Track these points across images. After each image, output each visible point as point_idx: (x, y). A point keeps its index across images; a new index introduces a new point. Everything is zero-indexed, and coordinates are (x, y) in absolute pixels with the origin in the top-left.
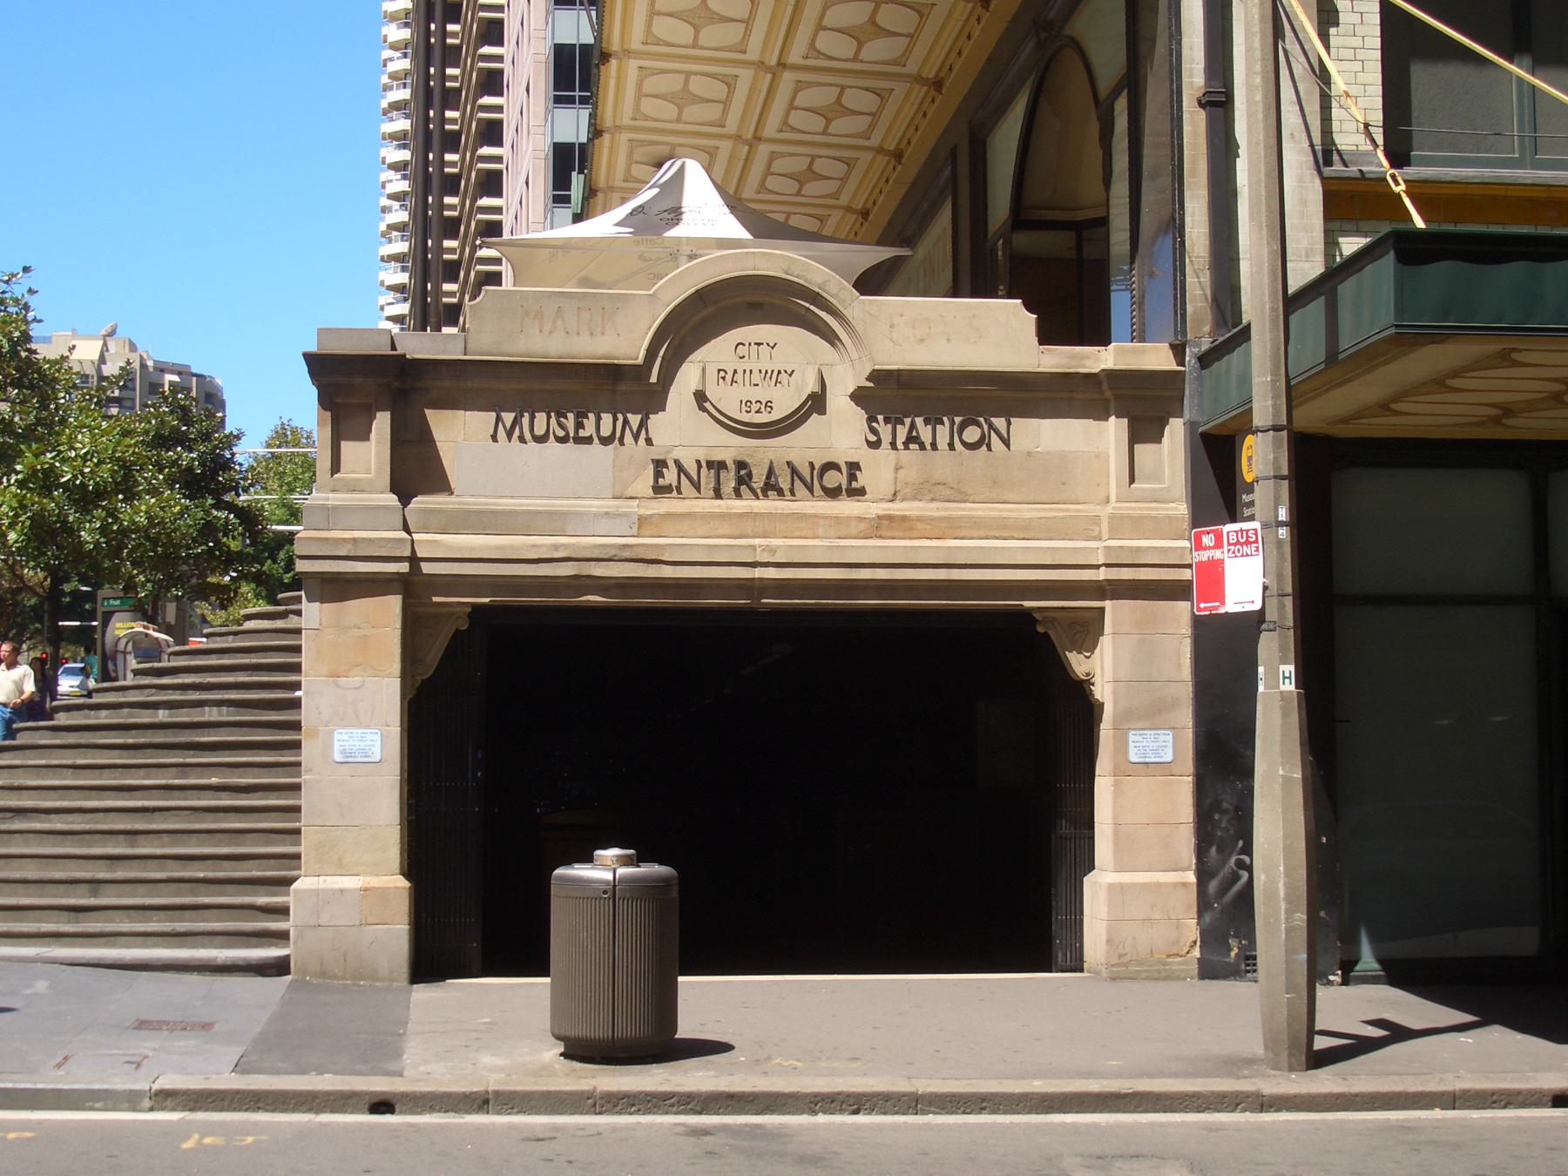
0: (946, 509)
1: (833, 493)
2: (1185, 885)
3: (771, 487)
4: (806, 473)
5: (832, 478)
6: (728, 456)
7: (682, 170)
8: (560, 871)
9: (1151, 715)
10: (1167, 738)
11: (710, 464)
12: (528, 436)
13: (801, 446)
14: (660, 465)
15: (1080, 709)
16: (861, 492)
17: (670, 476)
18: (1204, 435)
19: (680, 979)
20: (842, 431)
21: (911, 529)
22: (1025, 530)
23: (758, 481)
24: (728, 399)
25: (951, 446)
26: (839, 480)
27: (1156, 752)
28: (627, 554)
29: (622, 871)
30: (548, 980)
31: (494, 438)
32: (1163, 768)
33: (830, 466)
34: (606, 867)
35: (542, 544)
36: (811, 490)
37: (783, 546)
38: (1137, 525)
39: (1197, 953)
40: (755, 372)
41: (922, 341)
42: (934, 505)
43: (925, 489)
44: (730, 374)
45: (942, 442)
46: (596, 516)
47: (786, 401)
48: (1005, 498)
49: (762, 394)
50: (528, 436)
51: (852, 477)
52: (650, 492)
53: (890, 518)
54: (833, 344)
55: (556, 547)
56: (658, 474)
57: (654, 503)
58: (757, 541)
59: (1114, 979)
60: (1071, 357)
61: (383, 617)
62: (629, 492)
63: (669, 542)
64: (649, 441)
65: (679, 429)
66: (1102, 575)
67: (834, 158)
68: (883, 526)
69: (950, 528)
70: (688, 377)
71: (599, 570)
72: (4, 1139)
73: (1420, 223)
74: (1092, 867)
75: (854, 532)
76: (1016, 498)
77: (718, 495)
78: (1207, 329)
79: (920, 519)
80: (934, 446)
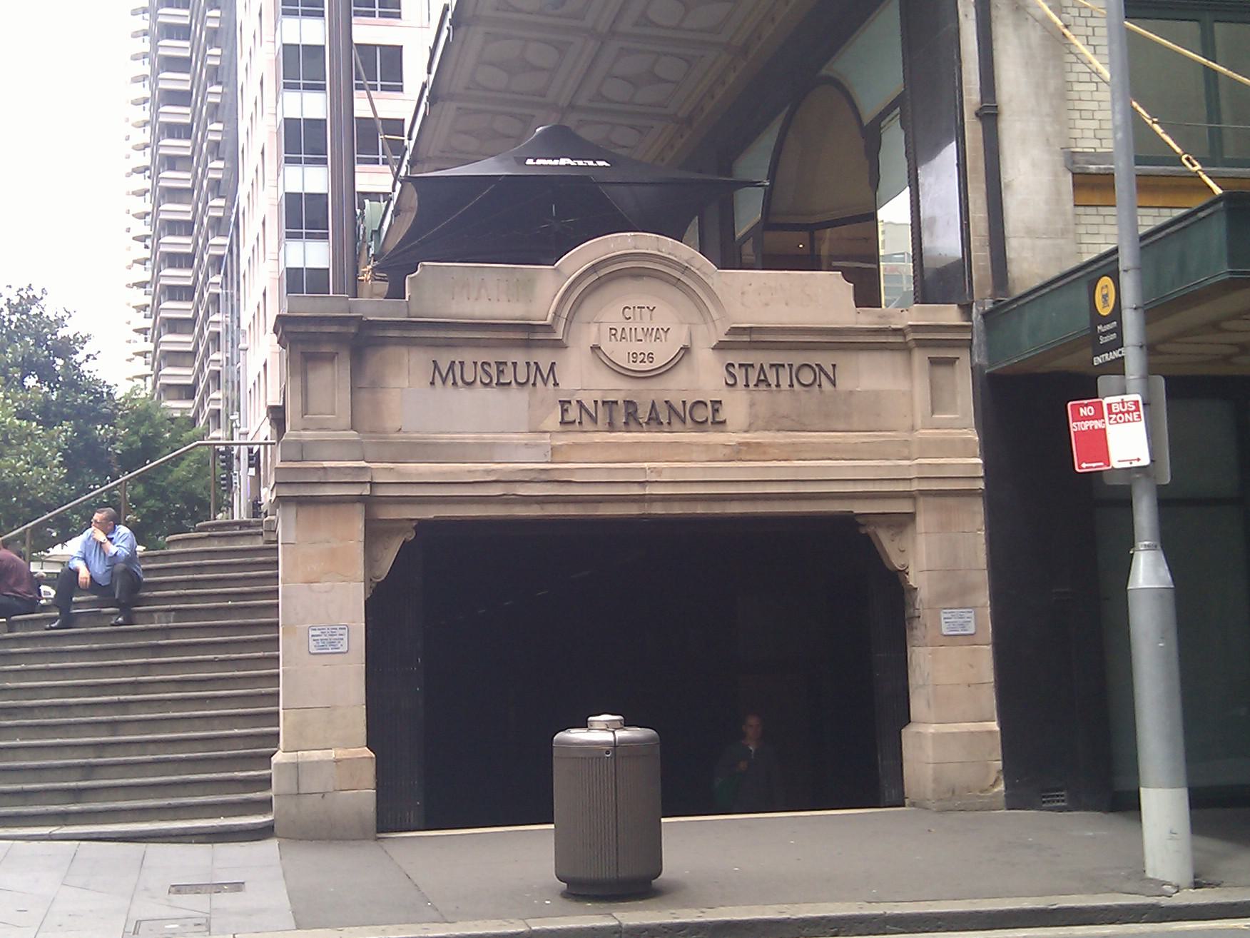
0: (790, 437)
1: (700, 425)
2: (991, 732)
3: (654, 421)
4: (680, 409)
5: (701, 414)
6: (619, 397)
8: (560, 736)
9: (956, 595)
10: (969, 615)
12: (460, 382)
13: (677, 388)
15: (895, 589)
17: (573, 413)
18: (991, 376)
19: (663, 820)
20: (705, 376)
21: (765, 453)
22: (853, 453)
23: (643, 413)
24: (619, 352)
25: (791, 385)
26: (705, 415)
27: (963, 626)
28: (544, 477)
29: (620, 734)
30: (552, 826)
31: (432, 383)
32: (969, 639)
34: (601, 731)
35: (475, 469)
36: (684, 421)
37: (666, 468)
38: (930, 447)
39: (1001, 787)
40: (639, 330)
41: (767, 305)
42: (780, 434)
43: (775, 422)
44: (620, 331)
45: (785, 383)
46: (517, 446)
47: (664, 352)
48: (835, 427)
49: (646, 347)
50: (460, 382)
51: (716, 411)
52: (558, 427)
53: (748, 444)
55: (488, 472)
56: (564, 411)
57: (563, 436)
58: (646, 465)
59: (943, 811)
61: (348, 534)
62: (543, 427)
63: (572, 466)
64: (556, 384)
65: (579, 376)
66: (915, 486)
67: (512, 115)
69: (794, 452)
70: (588, 335)
74: (907, 720)
75: (721, 456)
76: (842, 427)
77: (611, 427)
78: (989, 292)
79: (771, 445)
80: (778, 385)
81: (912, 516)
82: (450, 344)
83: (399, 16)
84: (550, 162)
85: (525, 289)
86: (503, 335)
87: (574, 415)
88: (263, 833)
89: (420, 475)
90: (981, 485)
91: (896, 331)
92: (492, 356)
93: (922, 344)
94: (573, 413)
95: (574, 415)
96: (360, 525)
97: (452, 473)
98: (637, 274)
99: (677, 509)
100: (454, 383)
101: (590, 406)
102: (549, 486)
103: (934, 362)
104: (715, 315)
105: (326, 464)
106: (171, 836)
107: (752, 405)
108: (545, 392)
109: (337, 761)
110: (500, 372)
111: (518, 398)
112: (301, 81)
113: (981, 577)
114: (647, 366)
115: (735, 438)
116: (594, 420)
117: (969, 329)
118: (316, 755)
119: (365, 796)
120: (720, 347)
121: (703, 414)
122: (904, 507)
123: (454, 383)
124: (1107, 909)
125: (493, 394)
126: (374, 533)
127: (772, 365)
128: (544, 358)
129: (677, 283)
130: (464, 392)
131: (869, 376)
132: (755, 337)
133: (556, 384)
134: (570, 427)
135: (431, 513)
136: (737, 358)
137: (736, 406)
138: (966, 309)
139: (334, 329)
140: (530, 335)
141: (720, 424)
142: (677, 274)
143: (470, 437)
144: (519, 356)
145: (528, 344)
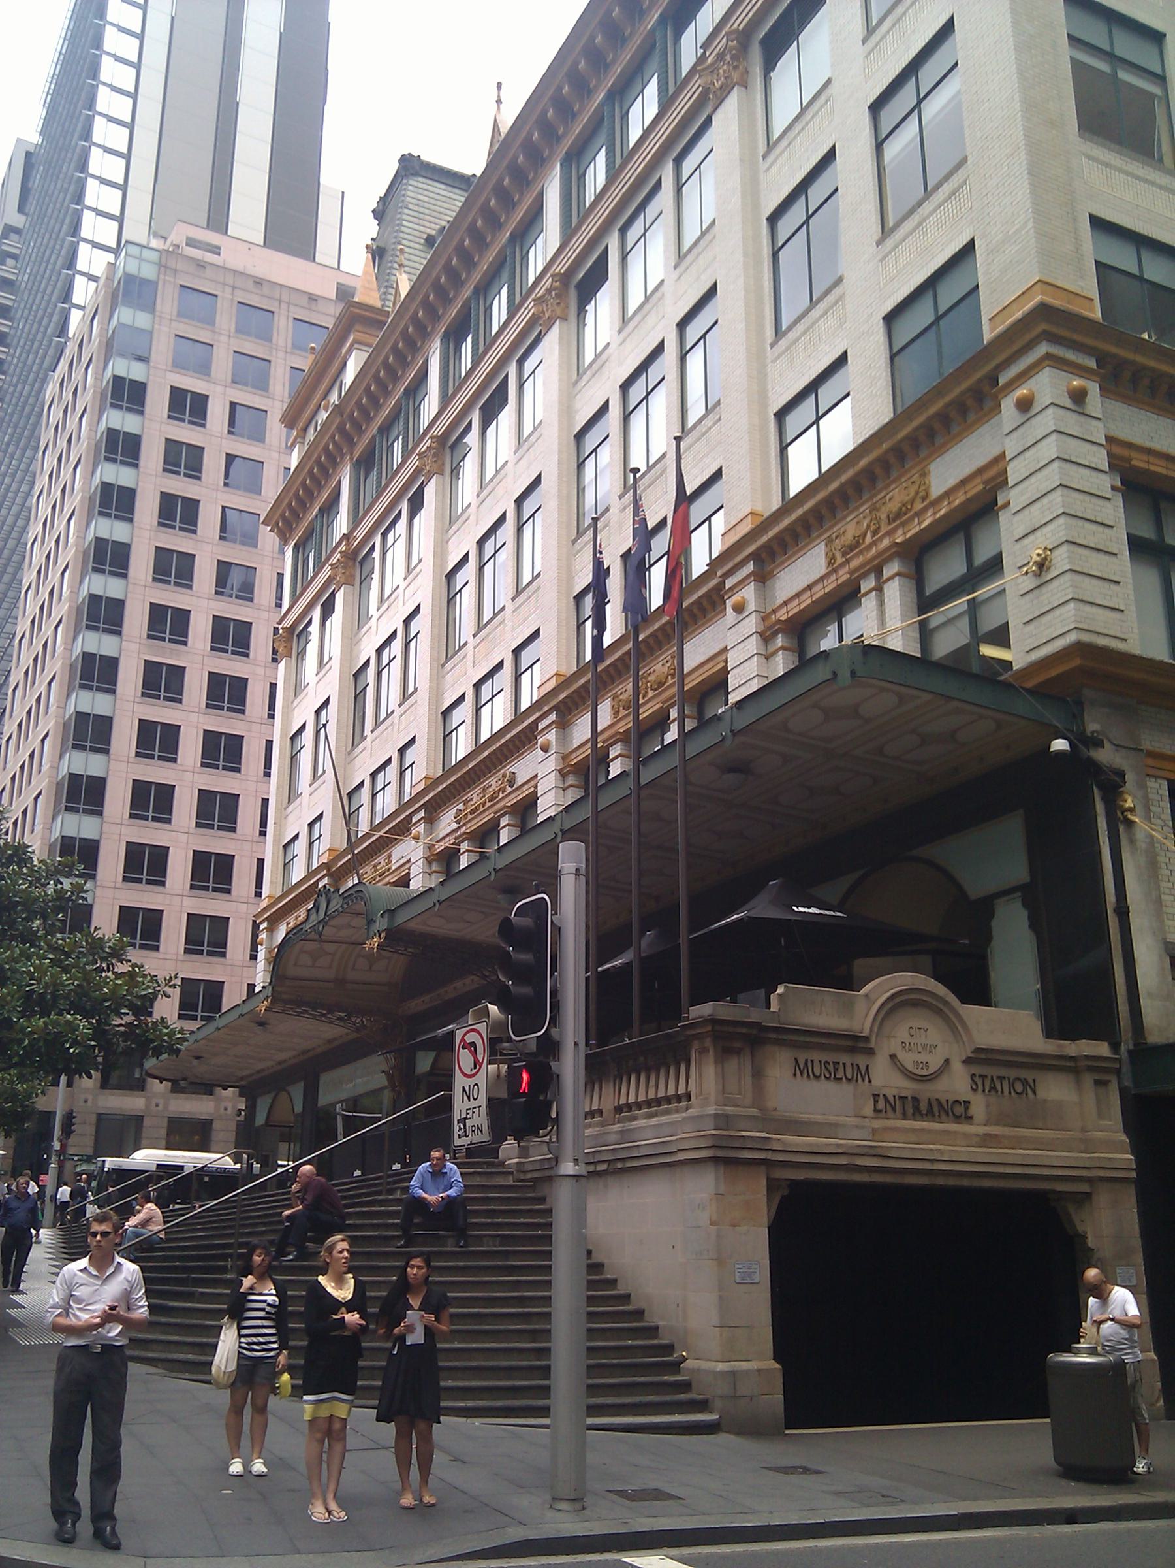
1: (958, 1119)
7: (598, 1278)
11: (900, 1097)
14: (876, 1096)
16: (971, 1117)
23: (923, 1107)
24: (908, 1060)
26: (958, 1111)
28: (872, 1152)
30: (1048, 1420)
33: (957, 1102)
36: (948, 1114)
37: (944, 1150)
39: (1161, 1402)
42: (1006, 1129)
47: (935, 1062)
51: (967, 1109)
54: (953, 1032)
55: (838, 1145)
56: (876, 1102)
60: (1060, 1046)
68: (987, 1140)
69: (1018, 1143)
71: (861, 1162)
72: (1161, 334)
73: (385, 1294)
79: (1004, 1137)
81: (1088, 1196)
82: (807, 1046)
83: (180, 701)
84: (806, 910)
85: (847, 1008)
86: (833, 1042)
87: (886, 1105)
88: (711, 1428)
89: (797, 1145)
90: (1134, 1174)
91: (1072, 1058)
92: (831, 1057)
93: (1091, 1069)
94: (881, 1104)
95: (886, 1105)
96: (764, 1182)
97: (817, 1145)
98: (915, 1004)
99: (952, 1182)
100: (808, 1076)
101: (891, 1099)
102: (875, 1159)
103: (1097, 1083)
104: (965, 1039)
105: (744, 1133)
106: (674, 1428)
107: (988, 1106)
108: (863, 1086)
109: (759, 1371)
110: (836, 1070)
111: (847, 1089)
112: (88, 744)
113: (1137, 1243)
114: (924, 1072)
115: (982, 1130)
116: (894, 1109)
117: (1119, 1061)
118: (744, 1365)
119: (776, 1399)
120: (967, 1061)
121: (959, 1110)
122: (1085, 1188)
123: (808, 1076)
124: (1110, 1508)
125: (831, 1086)
126: (772, 1185)
127: (998, 1077)
128: (862, 1060)
129: (939, 1012)
130: (814, 1083)
131: (1056, 1090)
132: (990, 1056)
133: (870, 1081)
134: (880, 1115)
135: (801, 1175)
136: (977, 1070)
137: (979, 1106)
138: (1115, 1047)
139: (744, 1030)
140: (856, 1044)
141: (969, 1118)
142: (941, 1006)
143: (820, 1118)
144: (845, 1059)
145: (852, 1050)
